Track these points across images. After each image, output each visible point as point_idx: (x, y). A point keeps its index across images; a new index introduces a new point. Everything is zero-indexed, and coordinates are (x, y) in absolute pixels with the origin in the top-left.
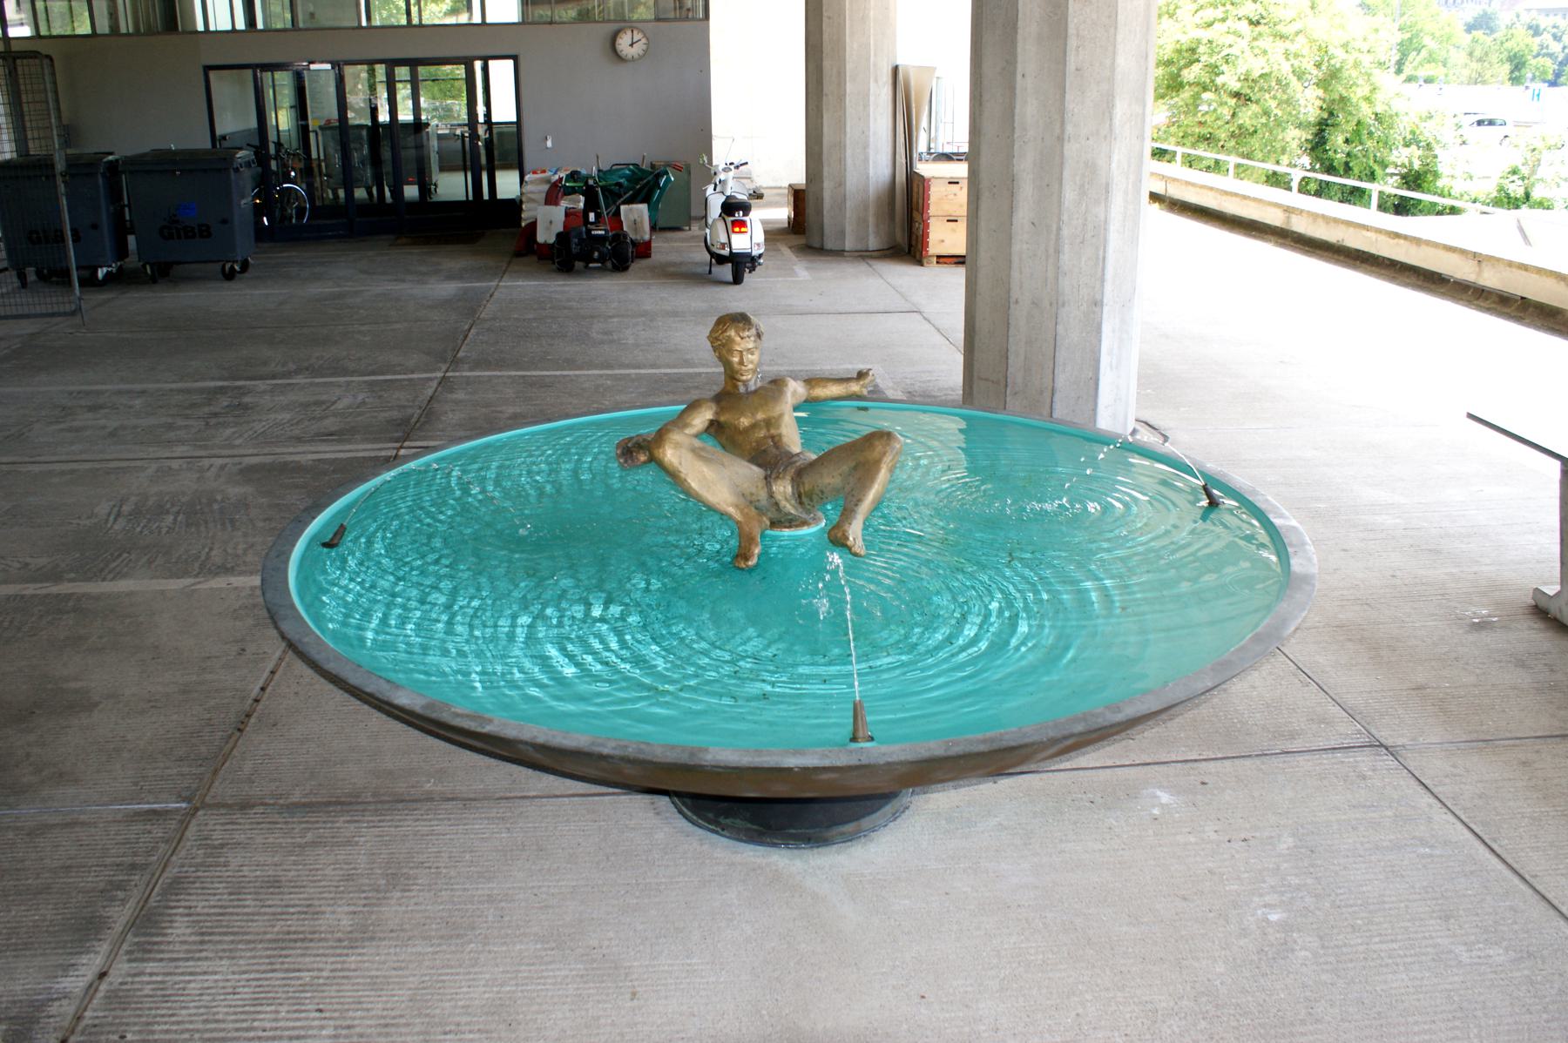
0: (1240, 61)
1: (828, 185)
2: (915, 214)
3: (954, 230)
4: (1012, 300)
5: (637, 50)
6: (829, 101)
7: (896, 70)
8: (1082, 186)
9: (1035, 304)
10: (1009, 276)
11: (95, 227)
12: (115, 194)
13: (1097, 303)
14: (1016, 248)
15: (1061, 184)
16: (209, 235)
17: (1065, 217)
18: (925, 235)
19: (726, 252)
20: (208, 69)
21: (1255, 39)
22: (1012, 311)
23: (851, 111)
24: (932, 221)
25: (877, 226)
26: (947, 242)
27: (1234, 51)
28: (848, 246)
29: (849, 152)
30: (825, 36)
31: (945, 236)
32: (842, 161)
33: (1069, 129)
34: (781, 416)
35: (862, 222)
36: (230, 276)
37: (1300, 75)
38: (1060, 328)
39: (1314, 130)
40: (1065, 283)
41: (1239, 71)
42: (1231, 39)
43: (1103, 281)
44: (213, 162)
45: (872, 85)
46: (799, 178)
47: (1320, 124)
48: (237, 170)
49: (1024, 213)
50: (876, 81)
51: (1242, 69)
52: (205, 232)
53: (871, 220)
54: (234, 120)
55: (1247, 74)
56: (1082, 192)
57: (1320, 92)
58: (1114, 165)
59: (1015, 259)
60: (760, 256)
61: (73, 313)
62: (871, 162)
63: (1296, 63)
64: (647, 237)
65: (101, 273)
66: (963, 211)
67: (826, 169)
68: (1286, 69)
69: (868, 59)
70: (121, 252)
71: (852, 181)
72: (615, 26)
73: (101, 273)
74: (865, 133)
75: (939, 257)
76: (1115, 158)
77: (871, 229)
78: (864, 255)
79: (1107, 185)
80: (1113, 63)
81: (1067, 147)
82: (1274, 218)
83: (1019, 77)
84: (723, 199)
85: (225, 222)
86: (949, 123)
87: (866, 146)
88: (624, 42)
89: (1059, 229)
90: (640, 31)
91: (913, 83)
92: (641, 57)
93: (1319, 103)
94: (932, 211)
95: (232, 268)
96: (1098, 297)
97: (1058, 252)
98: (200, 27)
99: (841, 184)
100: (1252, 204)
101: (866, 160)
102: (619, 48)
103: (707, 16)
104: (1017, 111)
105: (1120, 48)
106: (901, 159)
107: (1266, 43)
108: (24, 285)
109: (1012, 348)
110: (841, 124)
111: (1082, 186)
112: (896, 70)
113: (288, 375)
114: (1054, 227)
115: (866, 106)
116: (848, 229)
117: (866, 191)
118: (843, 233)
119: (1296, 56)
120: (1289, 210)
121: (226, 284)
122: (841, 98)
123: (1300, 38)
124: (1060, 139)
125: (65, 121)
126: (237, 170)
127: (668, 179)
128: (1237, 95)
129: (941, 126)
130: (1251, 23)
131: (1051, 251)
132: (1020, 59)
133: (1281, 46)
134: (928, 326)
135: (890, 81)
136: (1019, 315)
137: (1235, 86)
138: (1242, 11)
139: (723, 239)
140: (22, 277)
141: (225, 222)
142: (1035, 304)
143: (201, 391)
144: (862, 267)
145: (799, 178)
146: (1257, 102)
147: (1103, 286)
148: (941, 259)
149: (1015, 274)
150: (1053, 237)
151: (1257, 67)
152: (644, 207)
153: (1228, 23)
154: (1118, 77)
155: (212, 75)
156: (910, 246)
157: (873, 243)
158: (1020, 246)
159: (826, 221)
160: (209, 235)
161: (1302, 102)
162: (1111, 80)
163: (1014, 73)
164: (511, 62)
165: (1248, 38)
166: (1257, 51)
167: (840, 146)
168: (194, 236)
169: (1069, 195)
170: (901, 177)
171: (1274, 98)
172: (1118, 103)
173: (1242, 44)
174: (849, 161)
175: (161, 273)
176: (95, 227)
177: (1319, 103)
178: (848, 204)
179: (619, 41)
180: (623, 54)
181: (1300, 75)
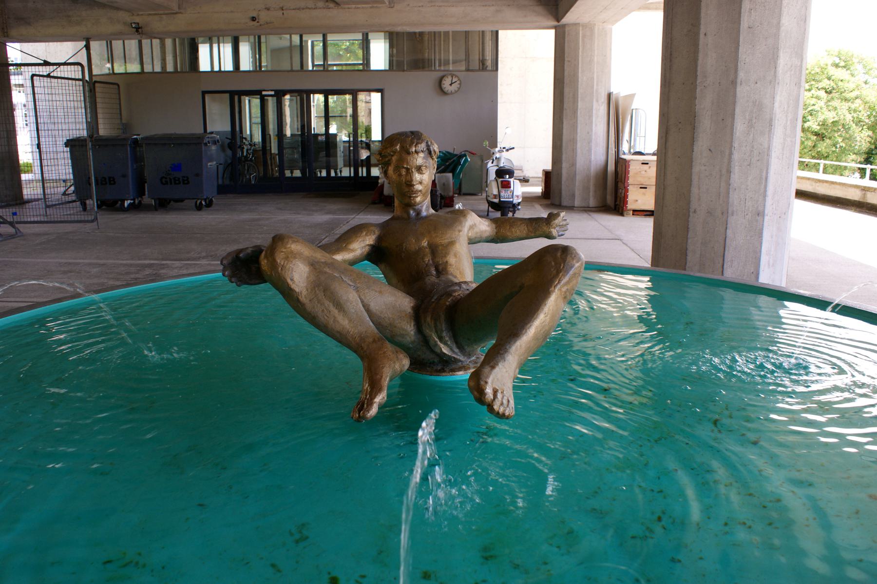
0: (820, 114)
1: (565, 165)
2: (620, 185)
3: (644, 194)
4: (692, 210)
5: (455, 87)
6: (567, 112)
7: (609, 96)
8: (750, 120)
9: (710, 213)
10: (689, 191)
11: (124, 176)
12: (138, 159)
13: (760, 214)
14: (696, 169)
15: (733, 118)
16: (188, 183)
17: (736, 145)
18: (626, 196)
19: (496, 201)
20: (204, 93)
21: (829, 101)
22: (691, 219)
23: (580, 119)
24: (630, 188)
25: (595, 191)
26: (639, 201)
27: (816, 108)
28: (577, 204)
29: (579, 145)
30: (566, 73)
31: (641, 197)
32: (574, 150)
33: (741, 75)
34: (452, 243)
35: (586, 189)
36: (199, 208)
37: (858, 122)
38: (729, 232)
39: (865, 156)
40: (734, 198)
41: (819, 119)
42: (813, 101)
43: (765, 196)
44: (194, 143)
45: (595, 103)
46: (549, 167)
47: (867, 153)
48: (206, 144)
49: (702, 144)
50: (597, 101)
51: (821, 118)
52: (186, 181)
53: (592, 188)
54: (218, 122)
55: (824, 121)
56: (751, 125)
57: (870, 133)
58: (777, 105)
59: (695, 178)
60: (519, 204)
61: (92, 221)
62: (593, 151)
63: (855, 115)
64: (451, 194)
65: (126, 203)
66: (653, 181)
67: (564, 157)
68: (849, 117)
69: (593, 87)
70: (141, 193)
71: (580, 162)
72: (442, 74)
73: (126, 203)
74: (589, 133)
75: (634, 211)
76: (778, 98)
77: (591, 194)
78: (586, 209)
79: (771, 120)
80: (779, 23)
81: (739, 89)
82: (854, 195)
83: (702, 36)
84: (497, 168)
85: (197, 175)
86: (644, 136)
87: (590, 142)
88: (446, 83)
89: (731, 154)
90: (456, 76)
91: (620, 103)
92: (456, 92)
93: (868, 139)
94: (630, 181)
95: (201, 203)
96: (761, 209)
97: (729, 172)
98: (169, 42)
99: (573, 164)
100: (838, 187)
101: (590, 150)
102: (444, 86)
103: (497, 69)
104: (700, 62)
105: (785, 11)
106: (612, 151)
107: (836, 103)
108: (85, 209)
109: (690, 247)
110: (574, 127)
111: (750, 120)
112: (609, 96)
113: (199, 259)
114: (727, 154)
115: (591, 117)
116: (577, 193)
117: (589, 169)
118: (573, 195)
119: (855, 111)
120: (865, 189)
121: (199, 213)
122: (575, 111)
123: (858, 101)
124: (734, 83)
125: (124, 121)
126: (206, 144)
127: (466, 160)
128: (816, 134)
129: (638, 138)
130: (826, 92)
131: (724, 171)
132: (702, 22)
133: (845, 105)
134: (625, 247)
135: (606, 102)
136: (697, 222)
137: (816, 128)
138: (821, 85)
139: (495, 192)
140: (84, 206)
141: (197, 175)
142: (710, 213)
143: (138, 265)
144: (585, 216)
145: (549, 167)
146: (830, 138)
147: (765, 200)
148: (636, 212)
149: (694, 190)
150: (726, 160)
151: (830, 116)
152: (450, 175)
153: (813, 91)
154: (782, 35)
155: (207, 97)
156: (616, 205)
157: (592, 203)
158: (698, 168)
159: (563, 187)
160: (188, 183)
161: (858, 139)
162: (777, 36)
163: (697, 34)
164: (379, 94)
165: (825, 100)
166: (830, 108)
167: (574, 141)
168: (179, 183)
169: (740, 127)
170: (611, 167)
171: (840, 136)
172: (781, 54)
173: (821, 103)
174: (579, 151)
175: (163, 205)
176: (124, 176)
177: (868, 139)
178: (578, 177)
179: (443, 82)
180: (446, 90)
181: (858, 122)
